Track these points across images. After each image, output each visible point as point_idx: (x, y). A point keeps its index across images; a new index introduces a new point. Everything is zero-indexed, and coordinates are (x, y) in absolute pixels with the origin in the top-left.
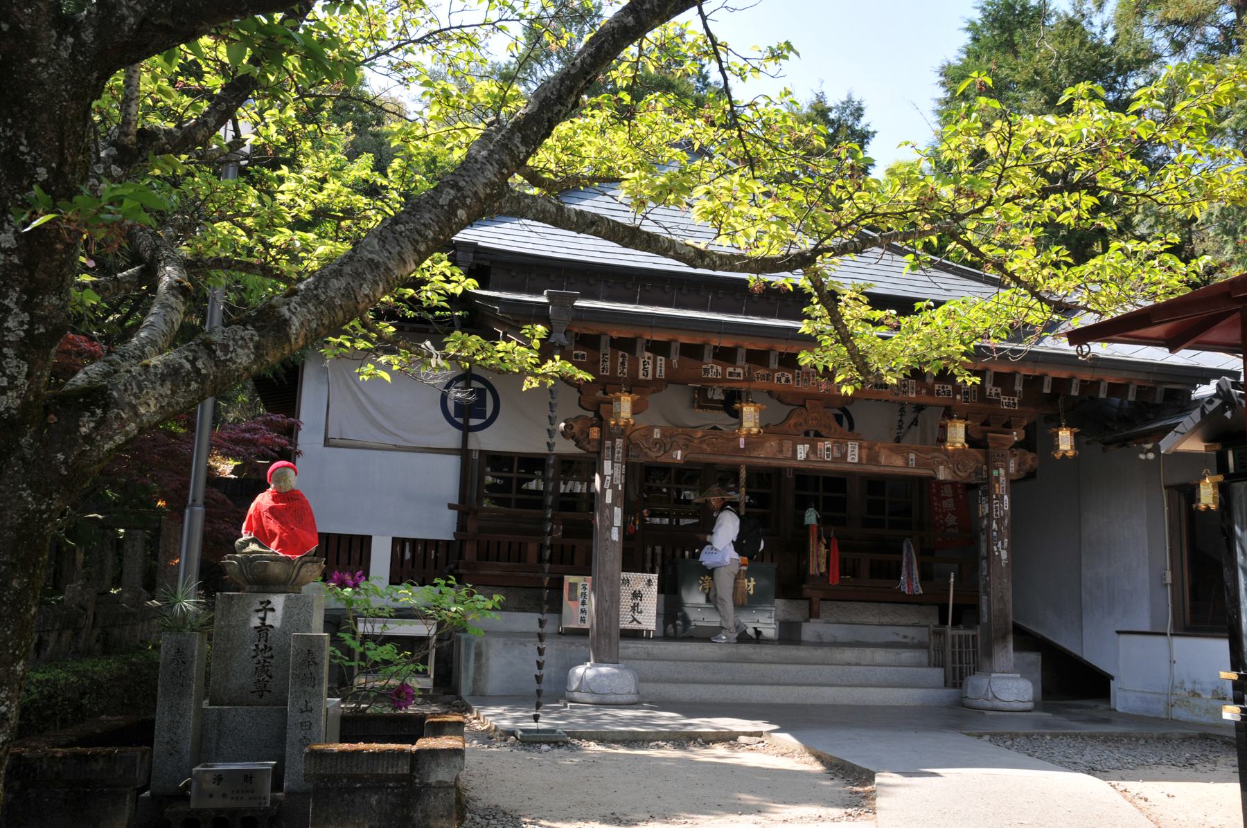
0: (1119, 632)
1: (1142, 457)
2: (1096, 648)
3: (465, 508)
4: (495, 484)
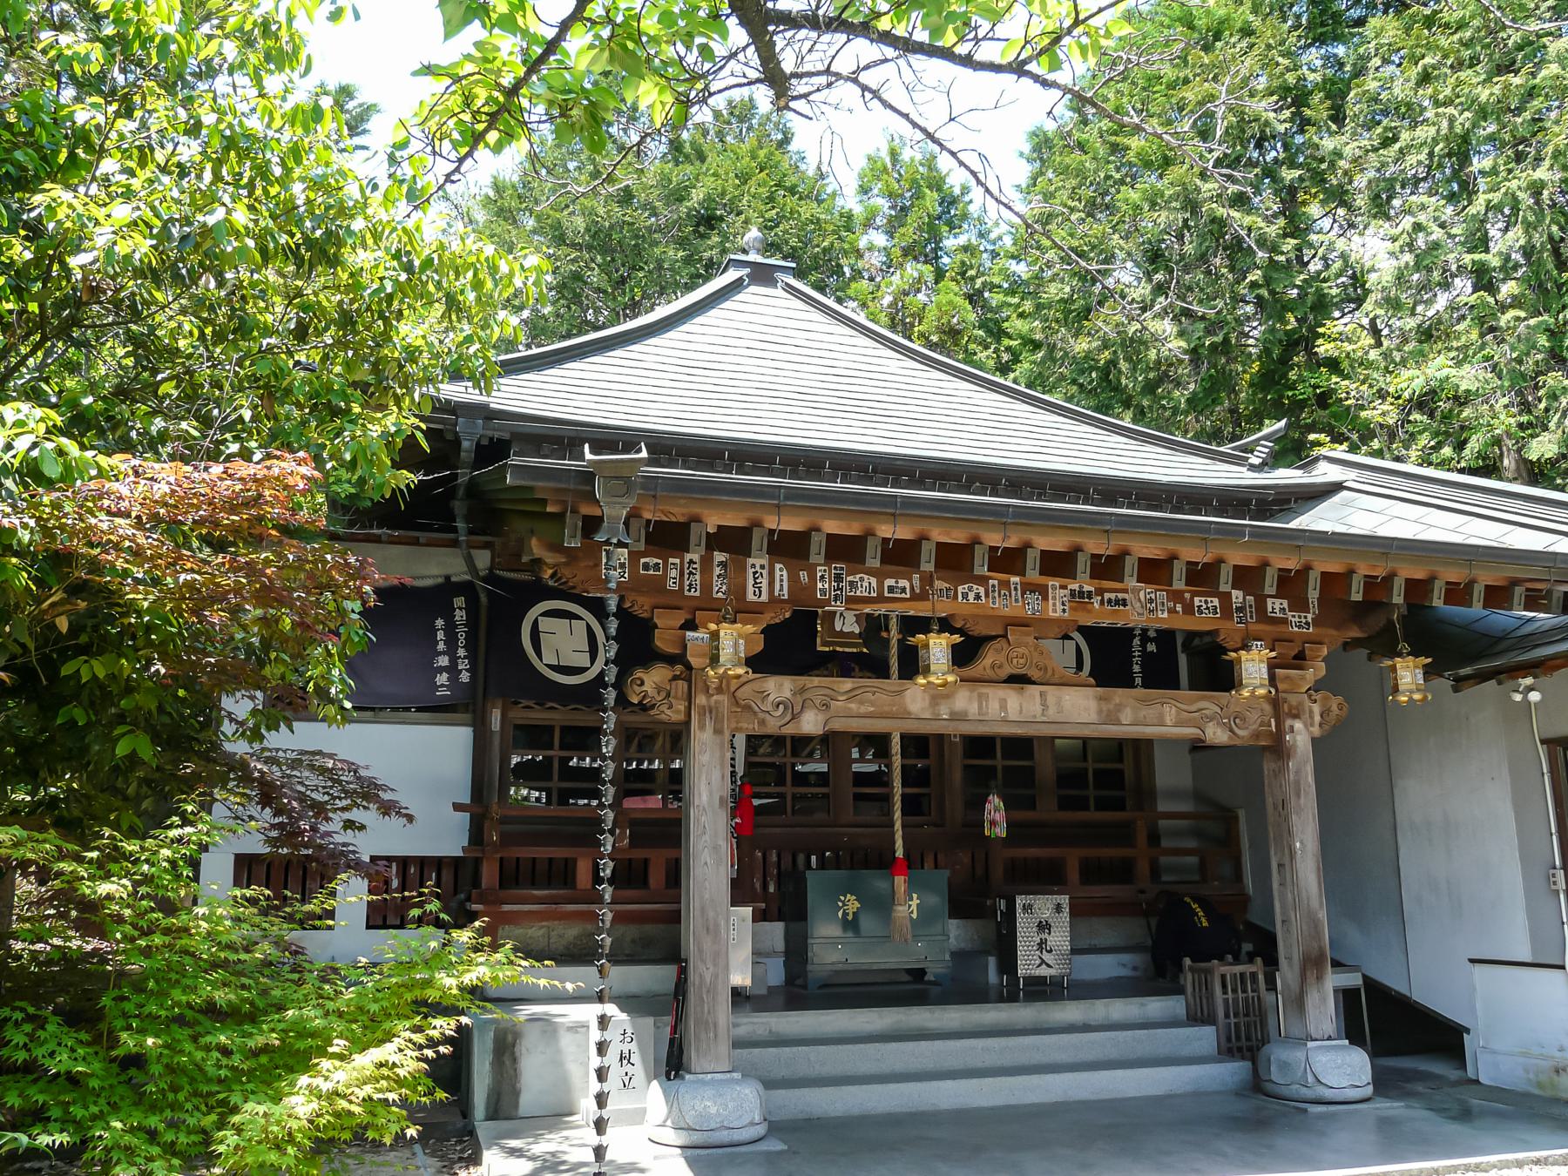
0: (1472, 961)
1: (1518, 697)
2: (1432, 982)
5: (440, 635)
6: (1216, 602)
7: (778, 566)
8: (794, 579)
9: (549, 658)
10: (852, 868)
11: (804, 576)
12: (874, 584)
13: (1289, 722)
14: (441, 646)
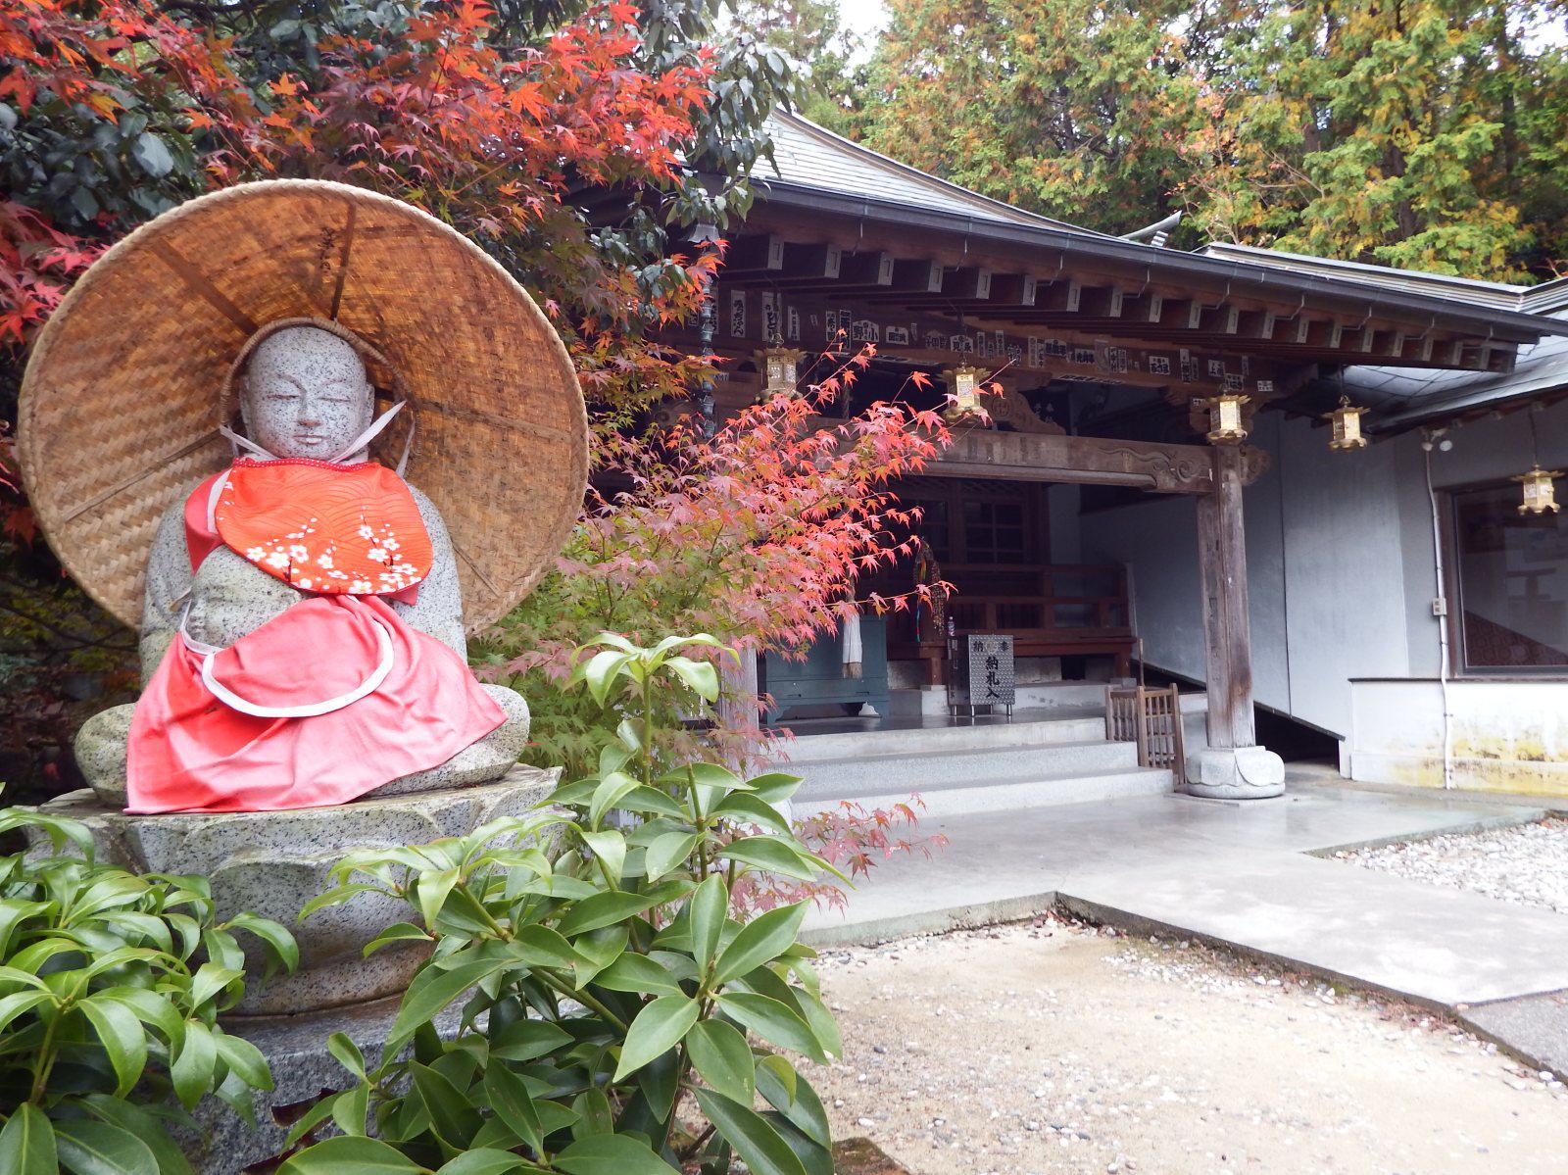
0: (1352, 680)
7: (790, 309)
11: (814, 319)
12: (877, 331)
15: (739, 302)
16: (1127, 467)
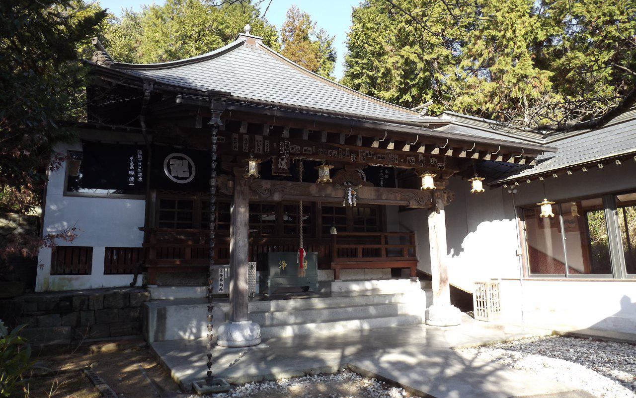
0: (502, 279)
3: (147, 229)
4: (288, 220)
5: (132, 163)
6: (414, 159)
7: (266, 141)
8: (271, 145)
9: (186, 163)
10: (283, 251)
11: (275, 144)
13: (437, 200)
14: (132, 167)
15: (246, 139)
16: (398, 198)
